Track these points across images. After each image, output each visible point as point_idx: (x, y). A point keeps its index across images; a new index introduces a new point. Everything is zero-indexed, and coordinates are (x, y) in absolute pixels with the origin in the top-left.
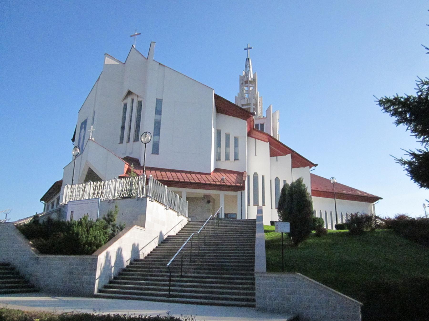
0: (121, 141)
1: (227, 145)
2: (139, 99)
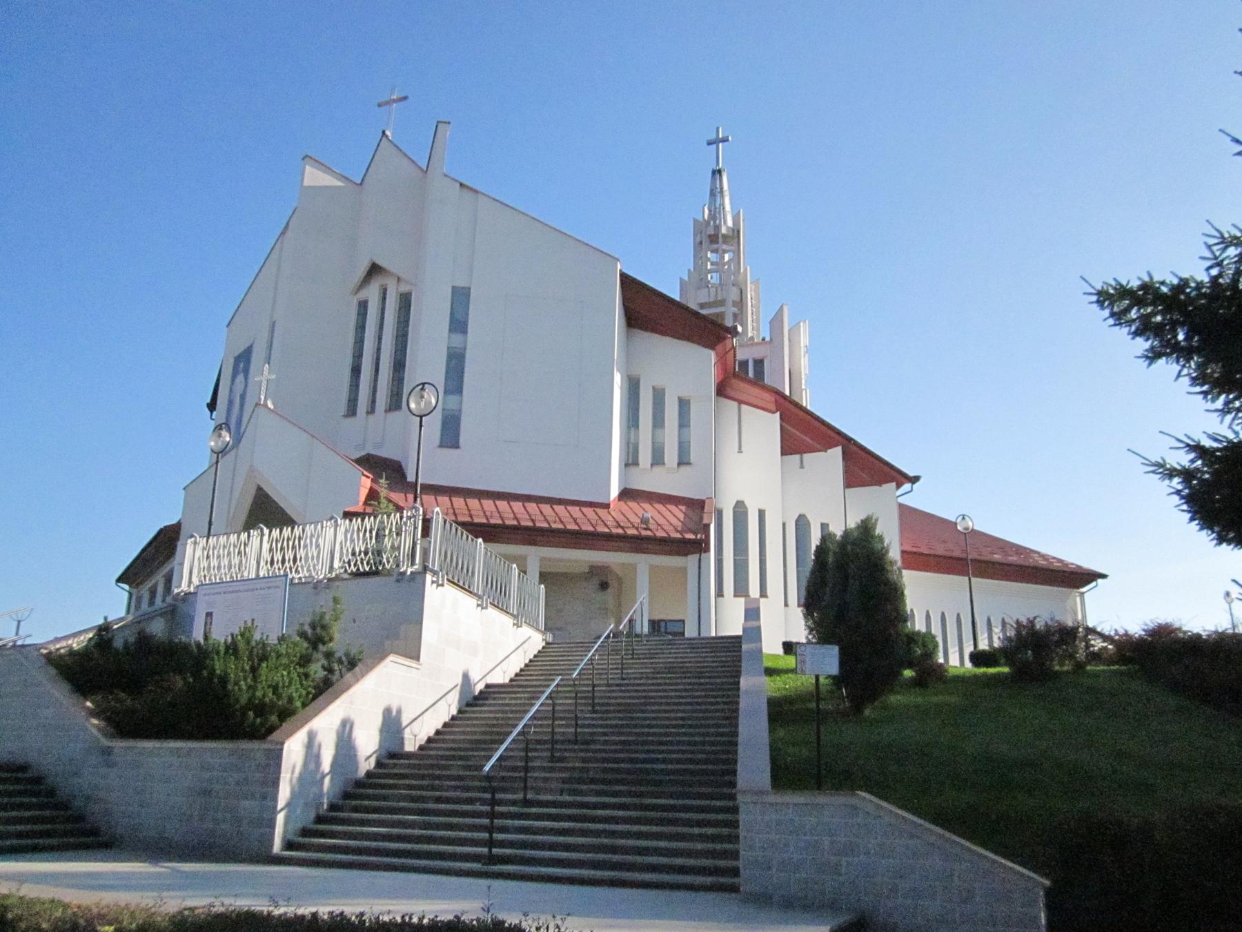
1: (658, 422)
2: (404, 288)
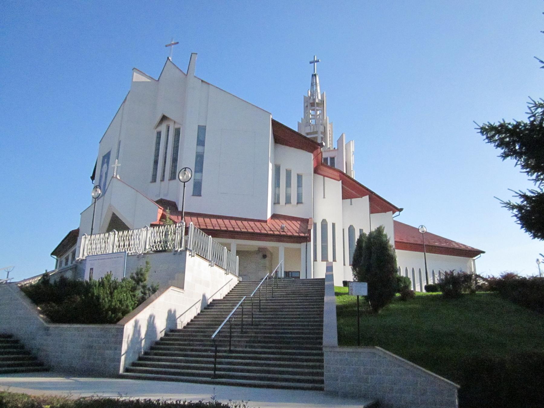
0: (154, 180)
1: (288, 185)
2: (177, 126)
